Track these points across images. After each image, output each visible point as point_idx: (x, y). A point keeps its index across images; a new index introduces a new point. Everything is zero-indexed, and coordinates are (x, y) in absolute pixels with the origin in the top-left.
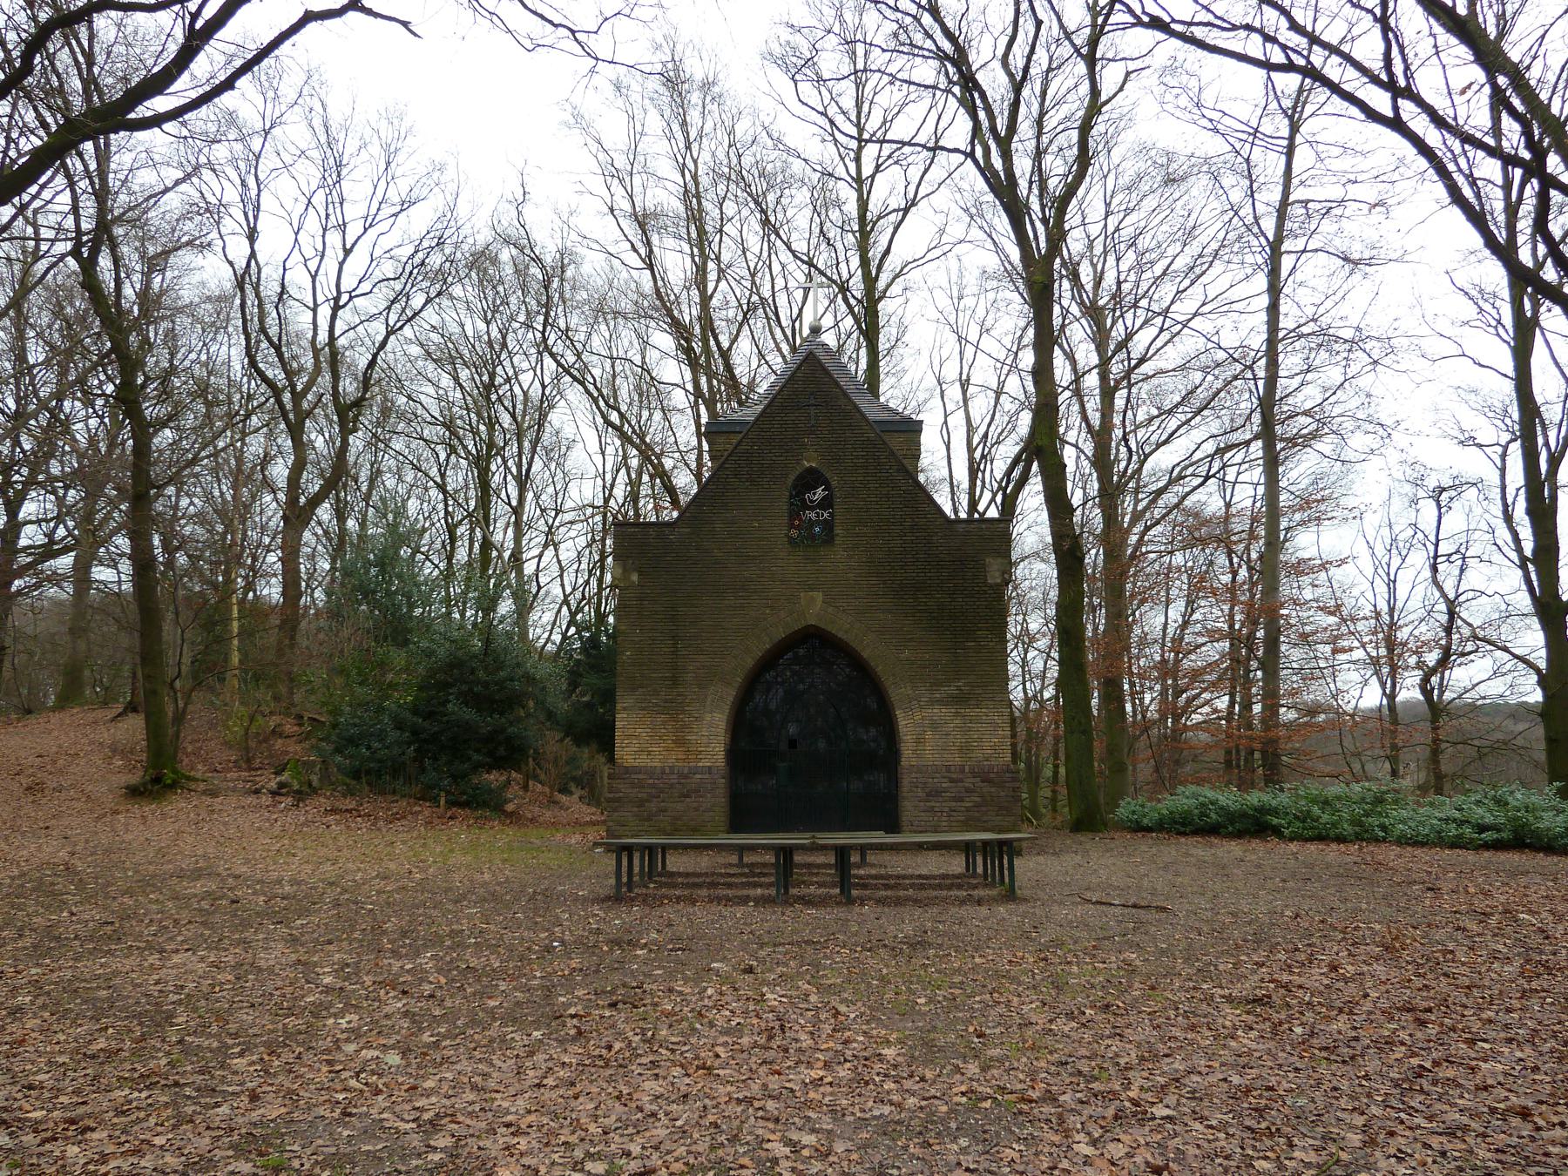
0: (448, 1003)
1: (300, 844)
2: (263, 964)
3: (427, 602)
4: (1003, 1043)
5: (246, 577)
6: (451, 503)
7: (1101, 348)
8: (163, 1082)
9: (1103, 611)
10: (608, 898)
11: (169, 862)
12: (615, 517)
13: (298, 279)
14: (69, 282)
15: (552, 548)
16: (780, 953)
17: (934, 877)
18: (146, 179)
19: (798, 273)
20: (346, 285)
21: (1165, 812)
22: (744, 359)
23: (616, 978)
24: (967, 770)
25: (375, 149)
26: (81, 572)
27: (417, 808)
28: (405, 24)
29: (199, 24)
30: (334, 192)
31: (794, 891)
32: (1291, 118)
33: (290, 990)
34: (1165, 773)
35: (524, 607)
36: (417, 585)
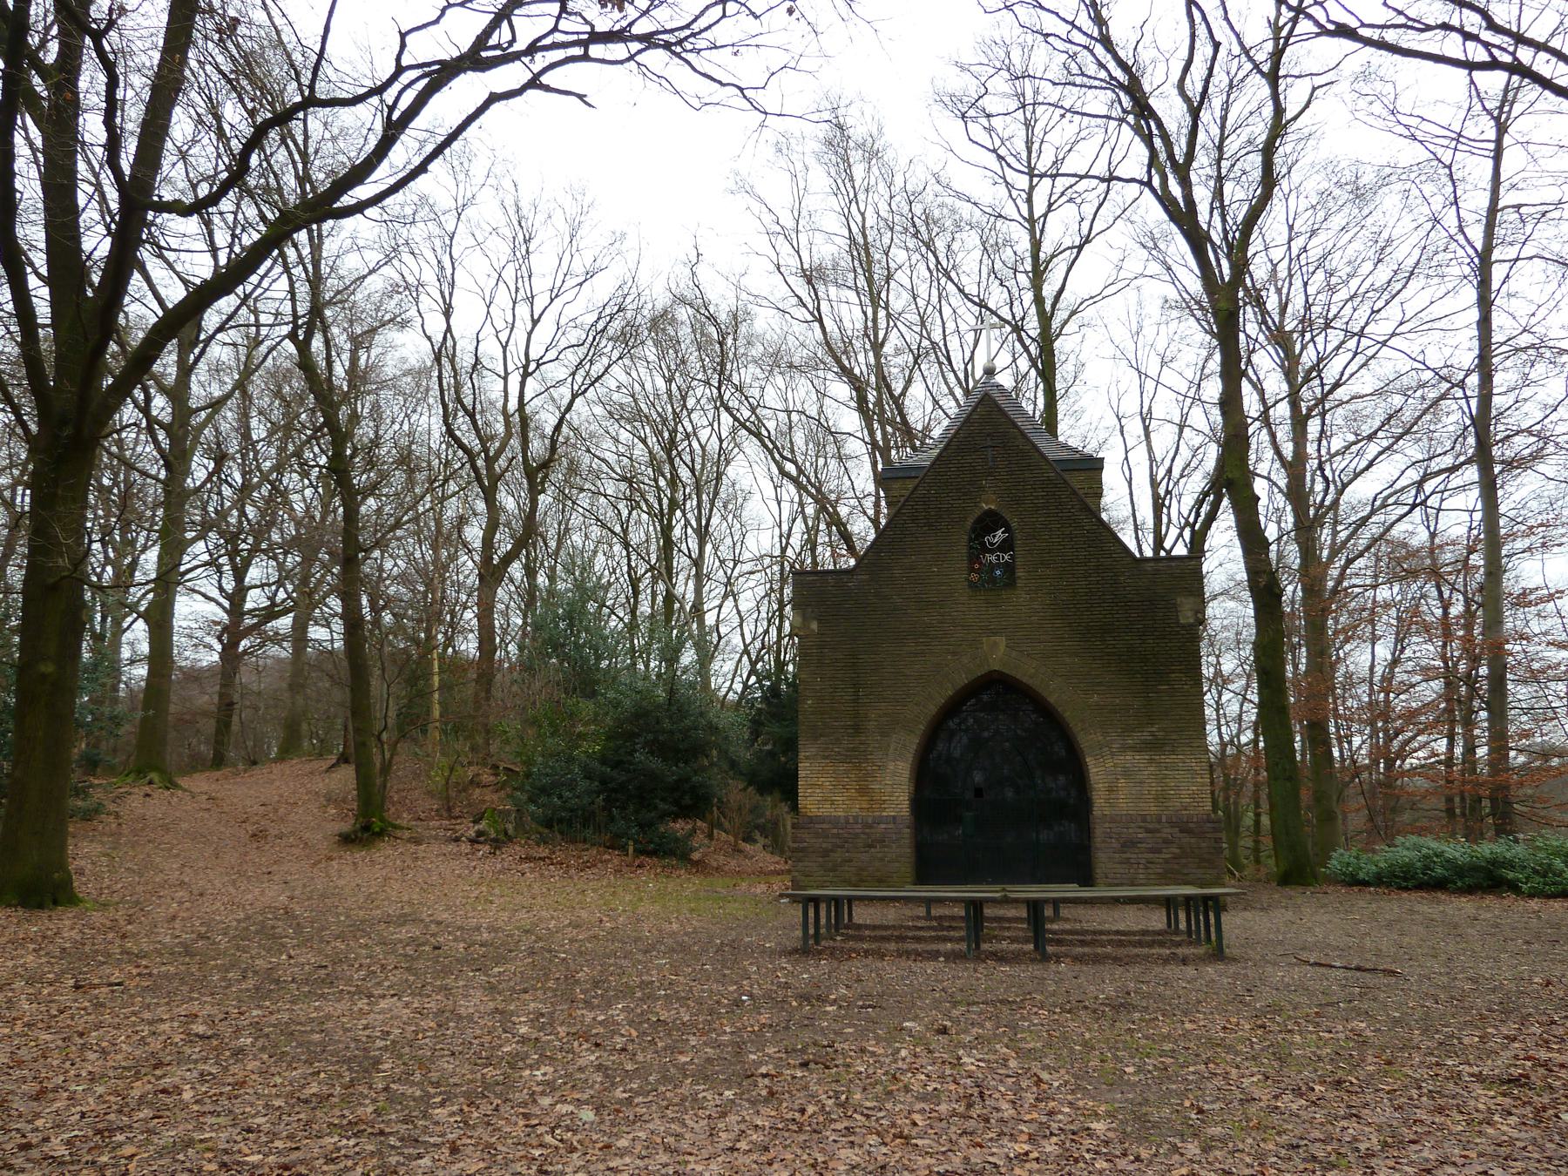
0: (640, 1058)
1: (497, 891)
2: (463, 1011)
3: (613, 654)
4: (1223, 1121)
5: (445, 633)
6: (634, 557)
7: (1289, 374)
8: (370, 1130)
9: (1304, 649)
10: (796, 951)
11: (378, 907)
12: (792, 566)
13: (491, 349)
14: (287, 364)
15: (731, 598)
16: (975, 1013)
17: (1134, 933)
18: (352, 264)
19: (968, 315)
20: (533, 355)
21: (1382, 865)
22: (918, 406)
23: (807, 1036)
24: (1164, 820)
25: (558, 219)
26: (300, 628)
27: (607, 857)
28: (581, 97)
29: (395, 116)
30: (523, 268)
31: (985, 946)
32: (1497, 119)
33: (488, 1038)
34: (1379, 820)
35: (706, 658)
36: (605, 638)
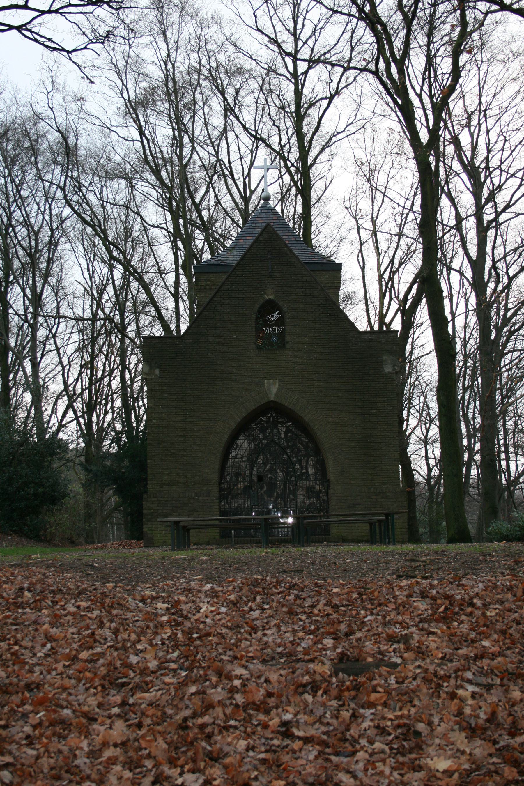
7: (477, 193)
19: (246, 140)
